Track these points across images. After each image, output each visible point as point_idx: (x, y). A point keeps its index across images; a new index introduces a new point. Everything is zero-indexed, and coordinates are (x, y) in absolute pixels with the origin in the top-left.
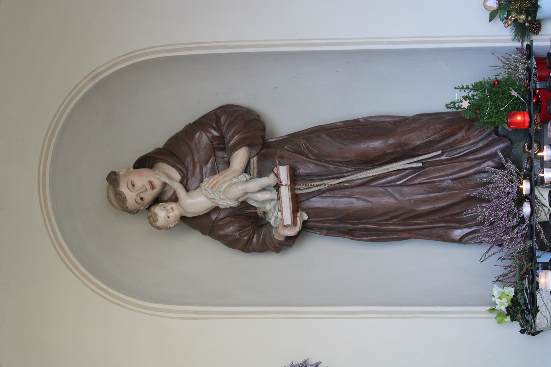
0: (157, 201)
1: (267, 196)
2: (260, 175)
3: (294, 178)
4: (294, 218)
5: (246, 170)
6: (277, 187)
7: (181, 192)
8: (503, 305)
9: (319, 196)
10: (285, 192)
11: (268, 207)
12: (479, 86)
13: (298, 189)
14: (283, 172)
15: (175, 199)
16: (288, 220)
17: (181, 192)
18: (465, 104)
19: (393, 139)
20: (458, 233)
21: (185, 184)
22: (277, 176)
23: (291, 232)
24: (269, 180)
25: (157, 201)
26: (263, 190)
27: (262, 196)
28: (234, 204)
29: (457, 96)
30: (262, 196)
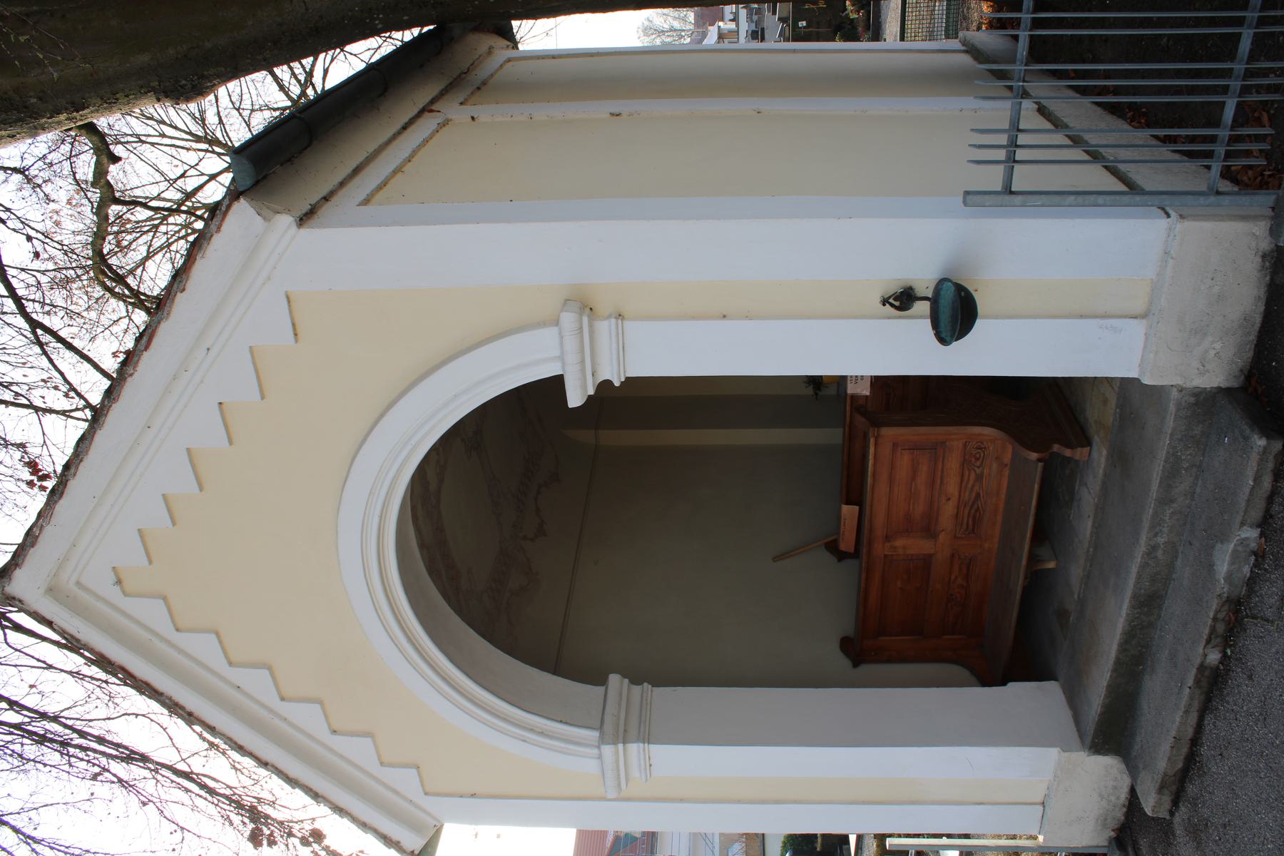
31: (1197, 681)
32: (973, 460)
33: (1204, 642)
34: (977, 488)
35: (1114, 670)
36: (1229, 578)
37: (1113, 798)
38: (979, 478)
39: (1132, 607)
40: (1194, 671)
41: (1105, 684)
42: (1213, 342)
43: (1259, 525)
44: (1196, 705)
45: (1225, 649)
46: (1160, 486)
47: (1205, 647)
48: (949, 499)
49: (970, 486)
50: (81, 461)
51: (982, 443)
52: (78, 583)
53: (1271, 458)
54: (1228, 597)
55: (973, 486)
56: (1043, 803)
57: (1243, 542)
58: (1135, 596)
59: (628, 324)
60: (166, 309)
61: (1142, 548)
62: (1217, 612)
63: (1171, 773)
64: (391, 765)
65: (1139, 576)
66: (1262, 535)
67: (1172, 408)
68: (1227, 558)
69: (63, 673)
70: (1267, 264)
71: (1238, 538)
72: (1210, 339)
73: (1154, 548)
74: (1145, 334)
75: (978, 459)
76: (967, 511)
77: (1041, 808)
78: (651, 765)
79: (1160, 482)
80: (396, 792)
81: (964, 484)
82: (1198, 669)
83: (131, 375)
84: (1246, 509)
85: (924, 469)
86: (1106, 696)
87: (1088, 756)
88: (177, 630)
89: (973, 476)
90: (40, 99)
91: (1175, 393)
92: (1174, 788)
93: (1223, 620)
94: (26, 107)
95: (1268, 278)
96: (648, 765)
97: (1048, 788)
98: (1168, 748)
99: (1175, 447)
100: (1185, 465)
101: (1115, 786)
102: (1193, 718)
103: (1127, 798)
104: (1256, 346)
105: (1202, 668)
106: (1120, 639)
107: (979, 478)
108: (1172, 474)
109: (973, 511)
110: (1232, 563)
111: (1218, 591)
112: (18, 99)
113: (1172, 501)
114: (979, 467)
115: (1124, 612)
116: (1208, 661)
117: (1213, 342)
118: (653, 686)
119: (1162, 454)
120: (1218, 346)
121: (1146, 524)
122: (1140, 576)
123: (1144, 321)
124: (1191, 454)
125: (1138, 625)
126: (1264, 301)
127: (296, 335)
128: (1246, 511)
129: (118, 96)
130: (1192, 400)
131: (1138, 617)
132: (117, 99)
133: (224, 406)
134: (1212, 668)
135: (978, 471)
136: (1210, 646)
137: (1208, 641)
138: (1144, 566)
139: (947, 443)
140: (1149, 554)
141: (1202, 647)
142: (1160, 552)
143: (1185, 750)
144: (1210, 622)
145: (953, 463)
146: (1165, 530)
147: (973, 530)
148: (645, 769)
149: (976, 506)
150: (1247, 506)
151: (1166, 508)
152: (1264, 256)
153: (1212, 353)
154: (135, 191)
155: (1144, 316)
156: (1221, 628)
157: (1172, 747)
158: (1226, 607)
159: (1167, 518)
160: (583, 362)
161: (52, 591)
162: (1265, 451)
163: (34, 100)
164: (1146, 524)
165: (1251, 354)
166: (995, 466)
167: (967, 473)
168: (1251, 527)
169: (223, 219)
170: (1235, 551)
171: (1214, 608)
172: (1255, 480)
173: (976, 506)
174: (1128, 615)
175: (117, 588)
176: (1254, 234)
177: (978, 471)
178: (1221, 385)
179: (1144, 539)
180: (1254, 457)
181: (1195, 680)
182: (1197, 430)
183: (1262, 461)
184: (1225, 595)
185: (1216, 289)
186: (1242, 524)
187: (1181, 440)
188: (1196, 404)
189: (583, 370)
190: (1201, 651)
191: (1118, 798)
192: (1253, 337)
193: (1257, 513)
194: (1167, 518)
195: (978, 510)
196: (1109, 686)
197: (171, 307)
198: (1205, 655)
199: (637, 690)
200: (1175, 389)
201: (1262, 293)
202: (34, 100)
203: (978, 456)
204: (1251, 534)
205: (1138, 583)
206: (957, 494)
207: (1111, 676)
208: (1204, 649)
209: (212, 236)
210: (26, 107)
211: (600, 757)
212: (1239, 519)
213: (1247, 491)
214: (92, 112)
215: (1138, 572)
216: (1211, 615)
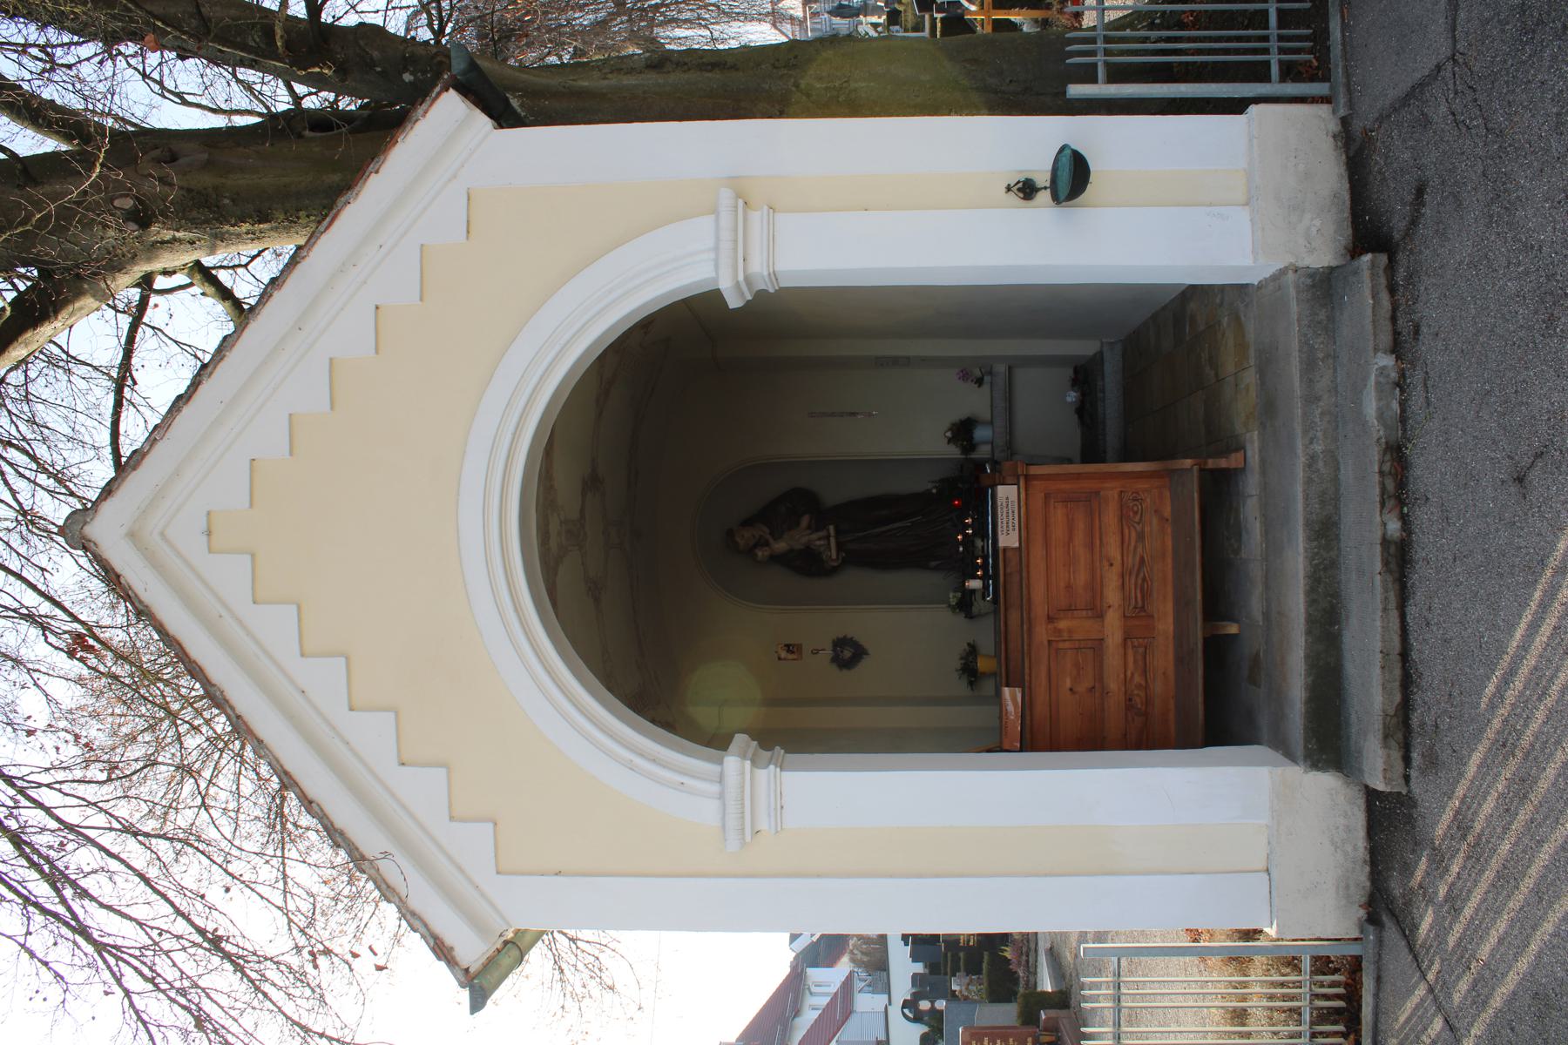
0: (755, 546)
1: (822, 542)
2: (817, 530)
3: (838, 532)
4: (838, 555)
5: (809, 527)
6: (828, 537)
7: (771, 540)
8: (953, 602)
9: (31, 452)
10: (833, 540)
11: (822, 549)
12: (942, 481)
13: (1337, 997)
14: (831, 528)
15: (767, 544)
16: (834, 556)
17: (771, 540)
18: (934, 491)
19: (1072, 402)
20: (933, 564)
21: (771, 534)
22: (828, 530)
23: (835, 564)
24: (822, 534)
25: (755, 546)
26: (819, 539)
27: (818, 543)
28: (802, 547)
29: (930, 486)
30: (818, 543)
31: (1386, 563)
32: (1131, 514)
33: (1378, 505)
34: (1139, 550)
35: (1309, 632)
36: (1381, 416)
37: (1349, 848)
38: (1141, 537)
39: (1309, 539)
40: (1378, 549)
41: (1302, 653)
42: (1312, 219)
43: (1393, 352)
44: (1393, 604)
45: (1402, 508)
46: (1301, 381)
47: (1381, 512)
48: (1111, 565)
49: (1132, 548)
50: (222, 359)
51: (1137, 493)
52: (162, 534)
53: (1381, 272)
54: (1387, 443)
55: (1135, 548)
56: (1268, 870)
57: (1382, 369)
58: (1308, 524)
59: (780, 217)
60: (357, 188)
61: (1301, 460)
62: (1382, 463)
63: (1391, 712)
64: (463, 820)
65: (1306, 497)
66: (1398, 358)
67: (1292, 292)
68: (1373, 394)
69: (47, 804)
70: (1339, 144)
71: (1376, 366)
72: (1308, 216)
73: (1312, 459)
74: (1251, 220)
75: (1136, 513)
76: (1133, 581)
77: (1265, 876)
78: (782, 807)
79: (1301, 376)
80: (461, 870)
81: (1125, 545)
82: (1381, 544)
83: (303, 258)
84: (1375, 332)
85: (1081, 525)
86: (1308, 674)
87: (1306, 772)
88: (254, 603)
89: (1133, 534)
90: (233, 200)
91: (1291, 276)
92: (1400, 736)
93: (1390, 473)
94: (218, 207)
95: (1344, 157)
96: (779, 807)
97: (1269, 843)
98: (1378, 671)
99: (1306, 335)
100: (1321, 355)
101: (1348, 827)
102: (1394, 615)
103: (1366, 848)
104: (1353, 223)
105: (1385, 542)
106: (1305, 585)
107: (1141, 537)
108: (1310, 365)
109: (1140, 581)
110: (1379, 399)
111: (1375, 436)
112: (214, 196)
113: (1319, 399)
114: (1138, 523)
115: (1301, 549)
116: (1389, 533)
117: (1312, 219)
118: (786, 752)
119: (1295, 345)
120: (1317, 223)
121: (1299, 430)
122: (1308, 495)
123: (1247, 207)
124: (1323, 343)
125: (1320, 564)
126: (1346, 178)
127: (468, 232)
128: (1375, 335)
129: (301, 213)
130: (1309, 281)
131: (1317, 554)
132: (298, 218)
133: (379, 311)
134: (1396, 543)
135: (1139, 528)
136: (1385, 511)
137: (1383, 504)
138: (1309, 482)
139: (1102, 493)
140: (1310, 466)
141: (1378, 513)
142: (1321, 464)
143: (1398, 672)
144: (1377, 478)
145: (1110, 517)
146: (1319, 434)
147: (1143, 607)
148: (775, 809)
149: (1142, 575)
150: (1375, 328)
151: (1314, 406)
152: (1334, 137)
153: (1314, 230)
154: (91, 907)
155: (1247, 204)
156: (1390, 485)
157: (1383, 668)
158: (1388, 457)
159: (1317, 420)
160: (736, 241)
161: (132, 536)
162: (1373, 265)
163: (226, 201)
164: (1299, 430)
165: (1350, 231)
166: (1155, 521)
167: (1126, 531)
168: (1385, 353)
169: (431, 105)
170: (1378, 383)
171: (1376, 458)
172: (1373, 297)
173: (1142, 575)
174: (1306, 550)
175: (205, 538)
176: (1320, 117)
177: (1139, 528)
178: (1331, 264)
179: (1301, 447)
180: (1366, 275)
181: (1382, 560)
182: (1322, 315)
183: (1373, 276)
184: (1383, 440)
185: (1301, 167)
186: (1376, 350)
187: (1309, 326)
188: (1313, 286)
189: (735, 250)
190: (1378, 519)
191: (1355, 848)
192: (1347, 214)
193: (1386, 338)
194: (1317, 420)
195: (1144, 579)
196: (1307, 657)
197: (361, 188)
198: (1384, 524)
199: (762, 774)
200: (1290, 272)
201: (1343, 170)
202: (226, 201)
203: (1135, 508)
204: (1387, 361)
205: (1308, 505)
206: (1119, 558)
207: (1306, 641)
208: (1381, 515)
209: (417, 120)
210: (218, 207)
211: (721, 779)
212: (1371, 344)
213: (1369, 312)
214: (272, 229)
215: (1304, 491)
216: (1376, 469)
